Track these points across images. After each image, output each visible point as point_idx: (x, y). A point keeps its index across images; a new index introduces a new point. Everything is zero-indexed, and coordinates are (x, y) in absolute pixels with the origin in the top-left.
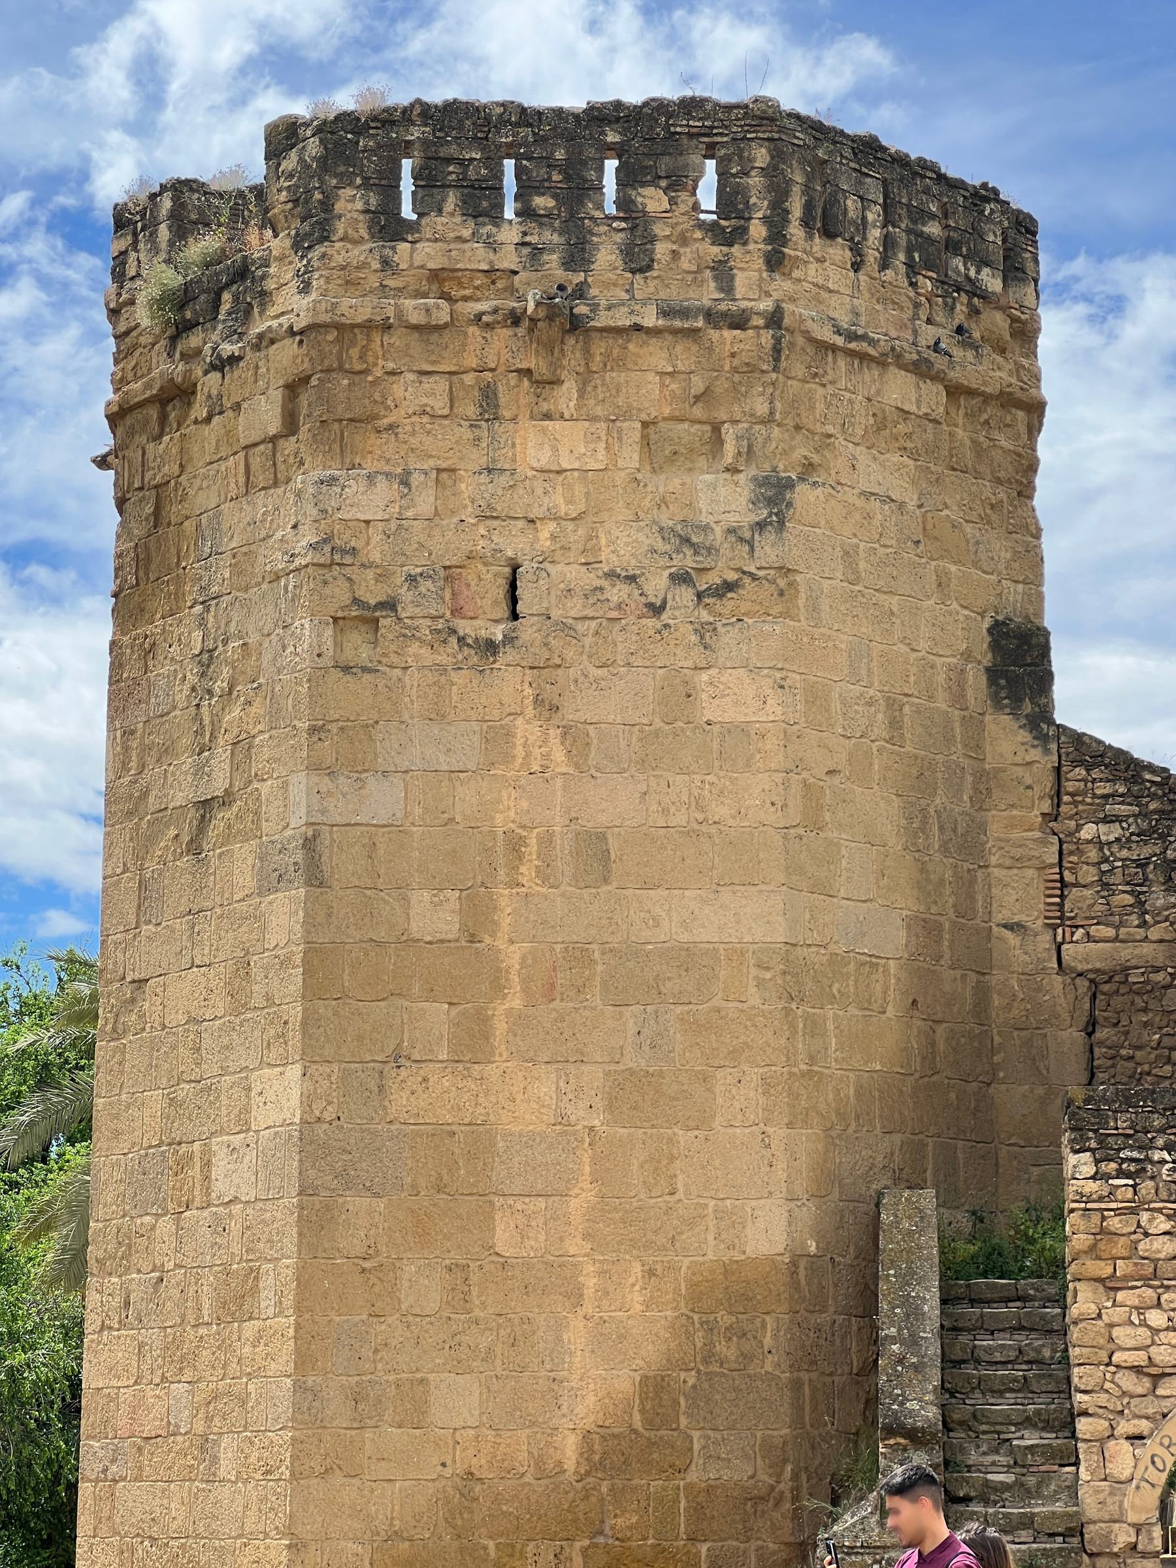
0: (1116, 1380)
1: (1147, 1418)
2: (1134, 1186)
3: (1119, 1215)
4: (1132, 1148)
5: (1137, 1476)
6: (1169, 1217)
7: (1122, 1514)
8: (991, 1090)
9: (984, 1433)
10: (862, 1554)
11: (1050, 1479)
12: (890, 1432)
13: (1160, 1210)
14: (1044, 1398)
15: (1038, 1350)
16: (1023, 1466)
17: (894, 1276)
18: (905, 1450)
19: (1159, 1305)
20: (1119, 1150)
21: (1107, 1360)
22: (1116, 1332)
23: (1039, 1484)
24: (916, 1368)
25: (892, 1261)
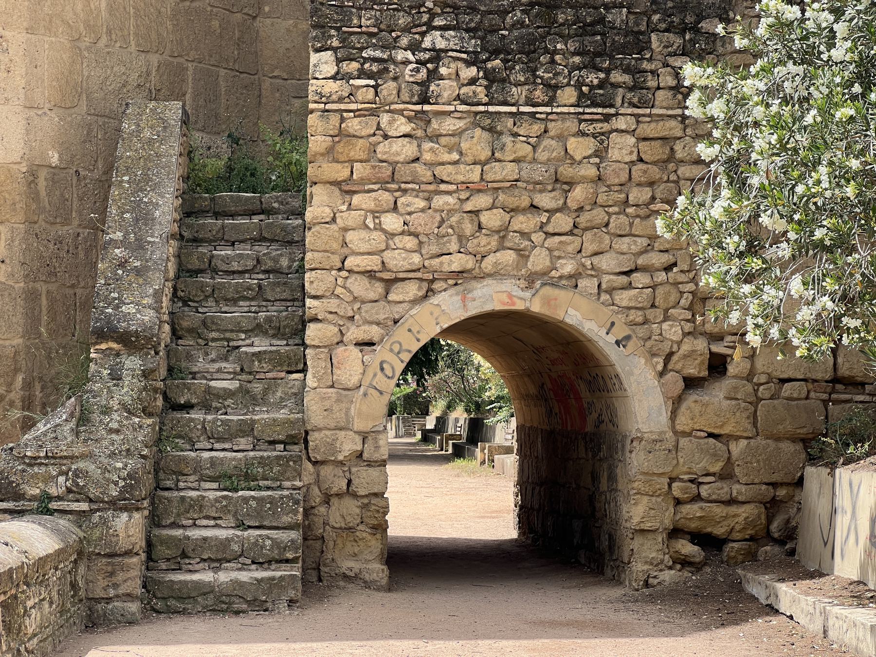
0: (348, 285)
1: (378, 324)
2: (376, 87)
3: (359, 116)
4: (375, 47)
5: (366, 383)
6: (409, 119)
7: (348, 422)
8: (257, 23)
9: (214, 340)
10: (46, 465)
11: (277, 386)
12: (101, 335)
13: (401, 112)
14: (278, 306)
15: (276, 260)
16: (250, 373)
17: (129, 182)
18: (118, 355)
19: (395, 208)
20: (361, 49)
21: (339, 265)
22: (350, 236)
23: (266, 391)
24: (138, 272)
25: (127, 168)
